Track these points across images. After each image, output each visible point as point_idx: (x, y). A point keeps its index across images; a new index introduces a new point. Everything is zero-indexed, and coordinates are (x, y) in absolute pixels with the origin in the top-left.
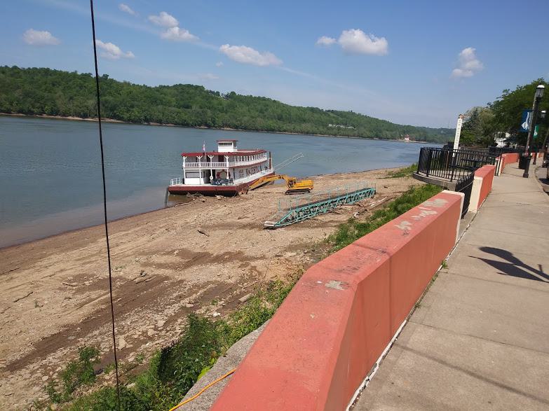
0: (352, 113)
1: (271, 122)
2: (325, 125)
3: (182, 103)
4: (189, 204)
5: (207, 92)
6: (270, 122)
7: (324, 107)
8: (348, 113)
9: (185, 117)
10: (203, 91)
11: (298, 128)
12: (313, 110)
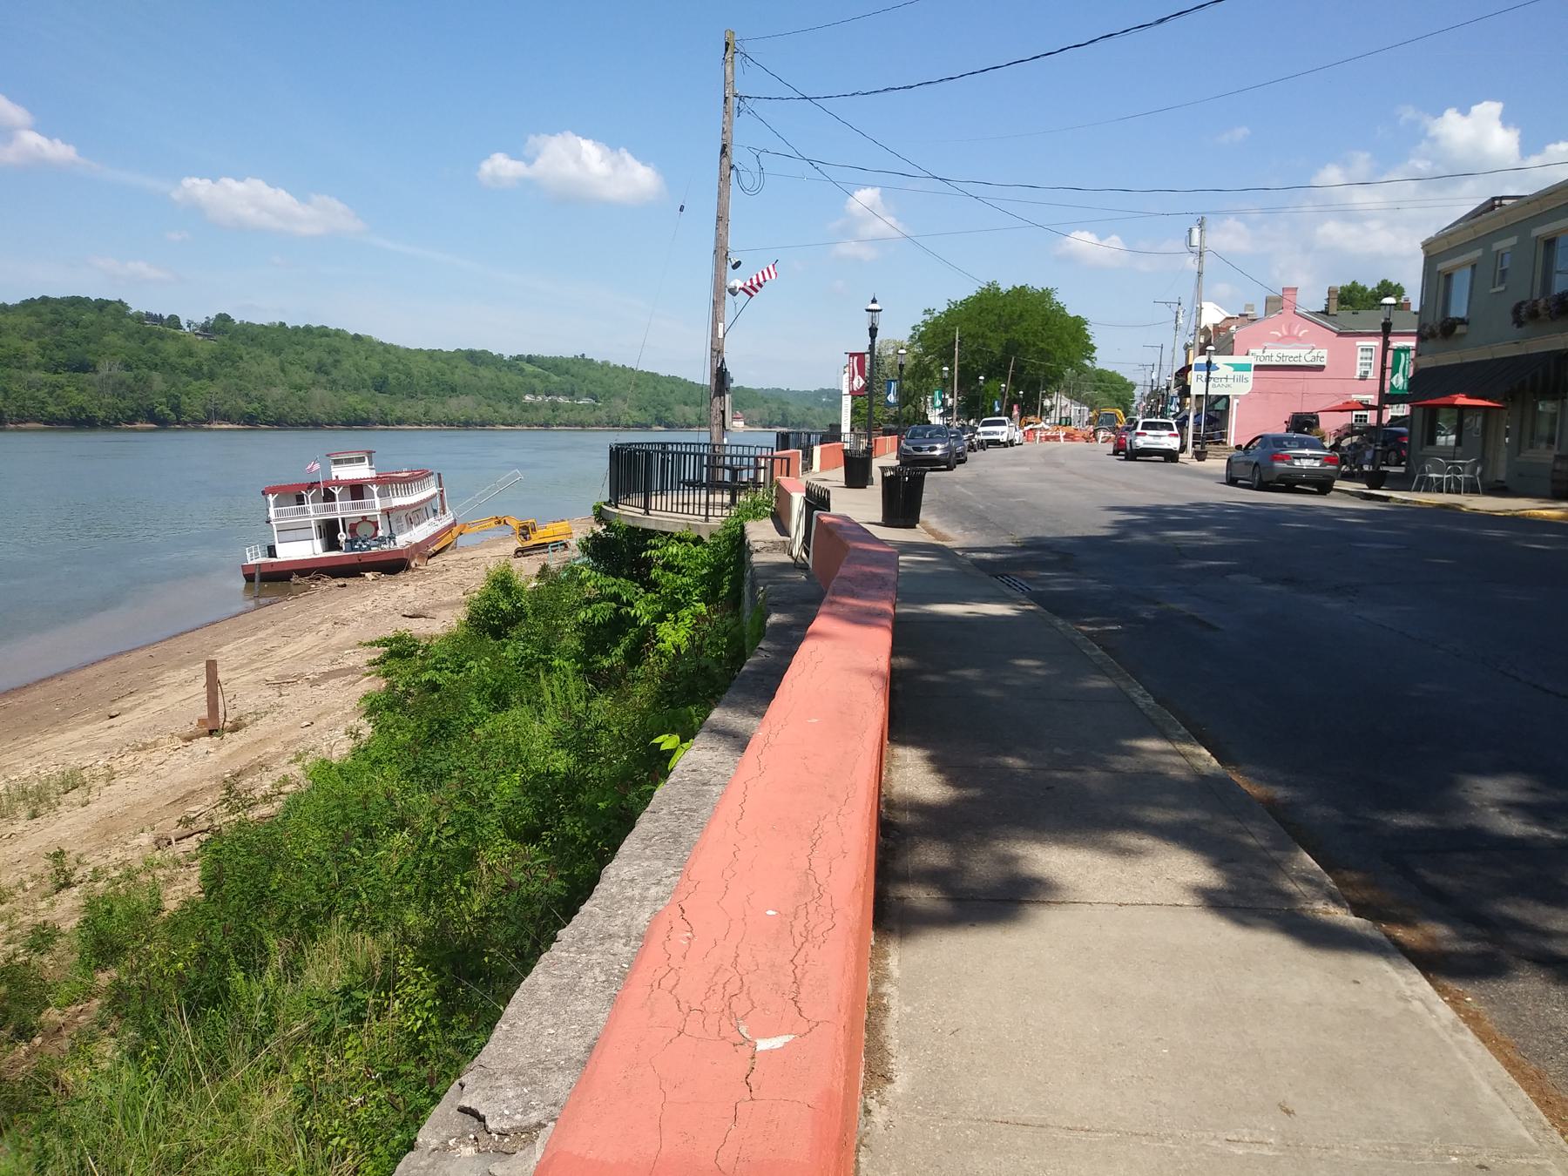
0: (584, 362)
1: (357, 398)
2: (513, 400)
3: (60, 355)
4: (296, 595)
5: (140, 318)
6: (352, 399)
7: (506, 345)
8: (575, 360)
9: (79, 399)
10: (125, 315)
11: (438, 411)
12: (475, 358)
